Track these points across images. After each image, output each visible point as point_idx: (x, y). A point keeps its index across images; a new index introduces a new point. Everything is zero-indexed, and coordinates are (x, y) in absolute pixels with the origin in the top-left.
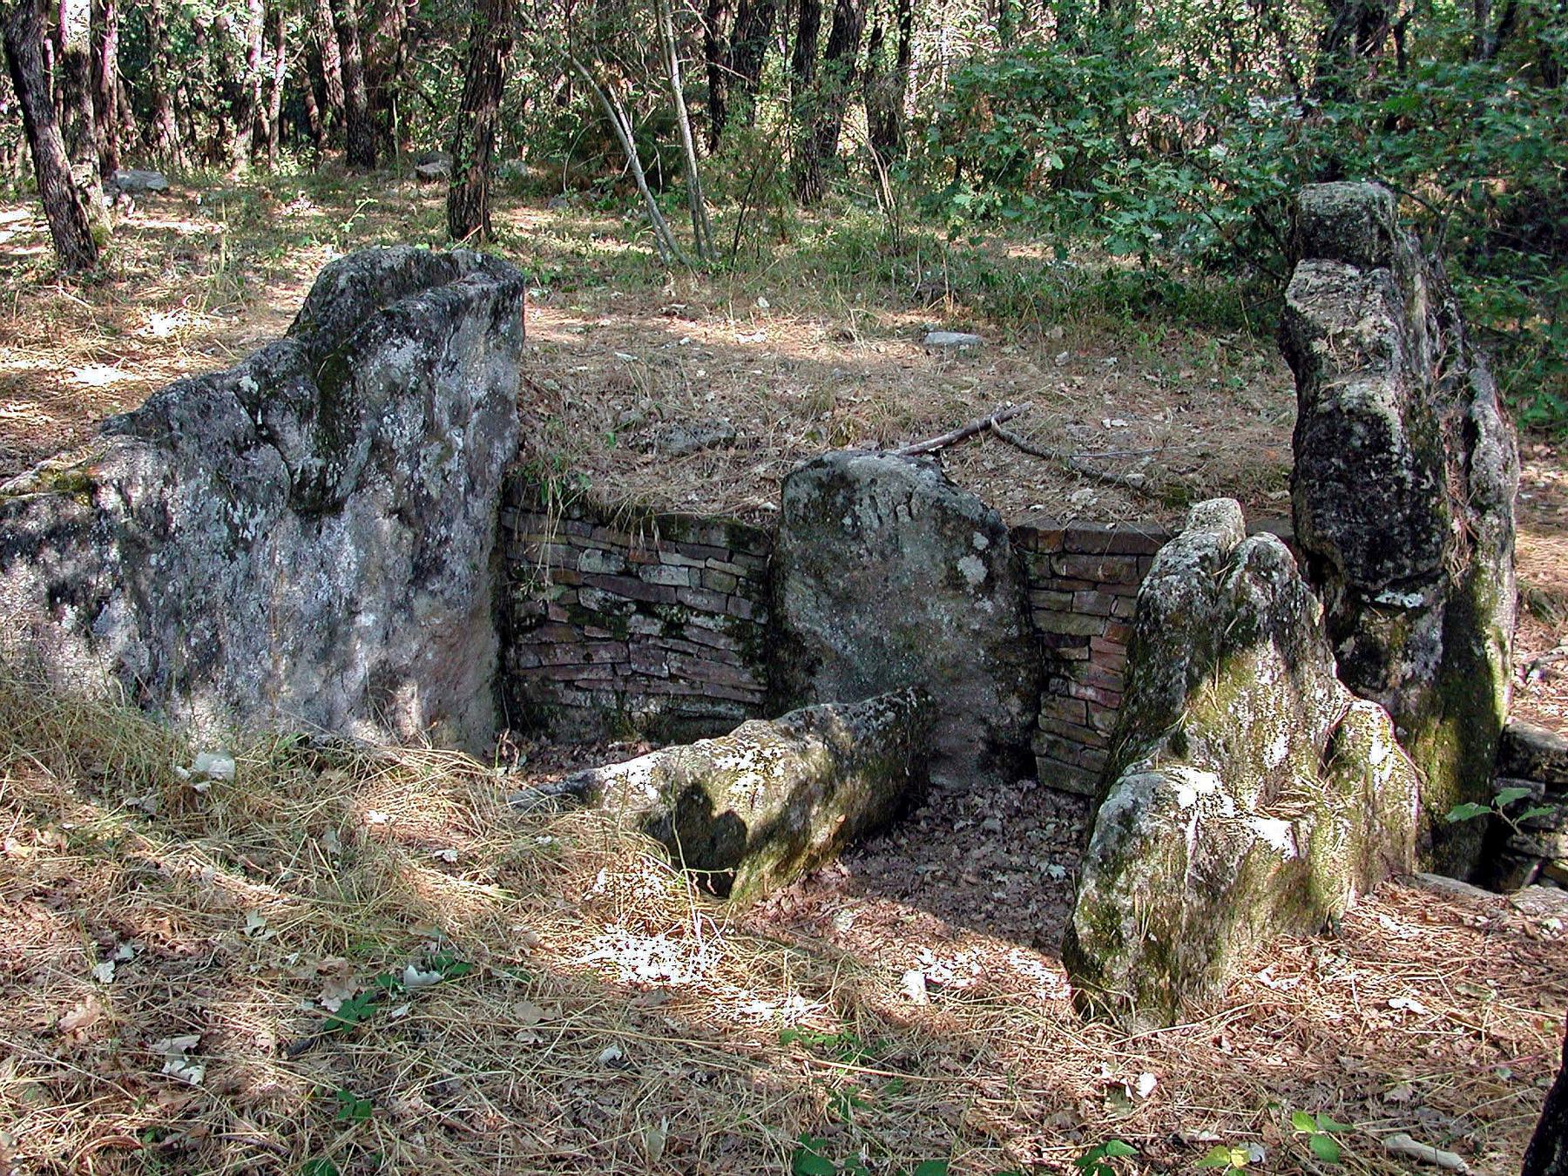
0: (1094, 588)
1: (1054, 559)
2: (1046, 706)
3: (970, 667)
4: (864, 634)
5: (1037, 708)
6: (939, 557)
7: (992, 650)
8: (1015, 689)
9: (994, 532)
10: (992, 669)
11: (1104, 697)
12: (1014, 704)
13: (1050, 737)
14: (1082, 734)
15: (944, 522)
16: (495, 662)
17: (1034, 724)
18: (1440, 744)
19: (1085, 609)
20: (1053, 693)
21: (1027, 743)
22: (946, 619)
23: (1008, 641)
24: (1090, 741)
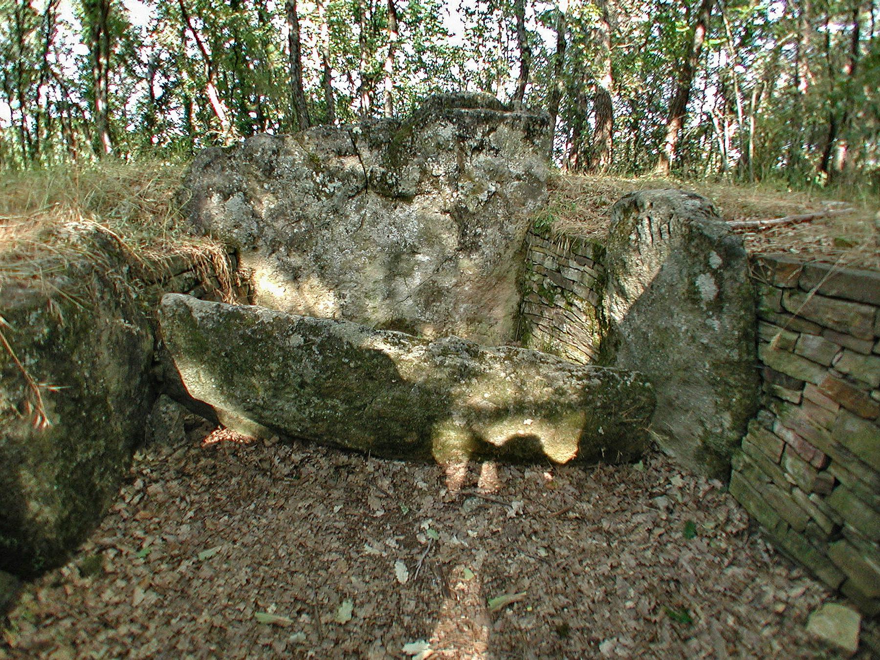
0: (820, 334)
1: (786, 294)
2: (753, 434)
3: (698, 375)
4: (639, 328)
5: (745, 431)
6: (685, 272)
7: (715, 366)
8: (728, 408)
9: (730, 253)
10: (713, 384)
11: (801, 446)
12: (727, 419)
13: (747, 459)
14: (774, 469)
15: (691, 239)
16: (516, 306)
17: (738, 443)
18: (830, 324)
19: (808, 353)
20: (760, 423)
21: (729, 455)
22: (684, 328)
23: (729, 362)
24: (777, 479)
